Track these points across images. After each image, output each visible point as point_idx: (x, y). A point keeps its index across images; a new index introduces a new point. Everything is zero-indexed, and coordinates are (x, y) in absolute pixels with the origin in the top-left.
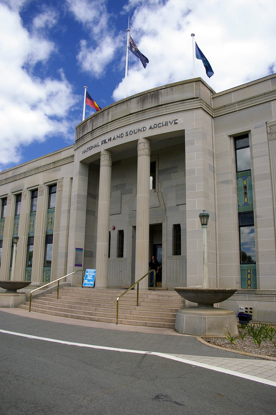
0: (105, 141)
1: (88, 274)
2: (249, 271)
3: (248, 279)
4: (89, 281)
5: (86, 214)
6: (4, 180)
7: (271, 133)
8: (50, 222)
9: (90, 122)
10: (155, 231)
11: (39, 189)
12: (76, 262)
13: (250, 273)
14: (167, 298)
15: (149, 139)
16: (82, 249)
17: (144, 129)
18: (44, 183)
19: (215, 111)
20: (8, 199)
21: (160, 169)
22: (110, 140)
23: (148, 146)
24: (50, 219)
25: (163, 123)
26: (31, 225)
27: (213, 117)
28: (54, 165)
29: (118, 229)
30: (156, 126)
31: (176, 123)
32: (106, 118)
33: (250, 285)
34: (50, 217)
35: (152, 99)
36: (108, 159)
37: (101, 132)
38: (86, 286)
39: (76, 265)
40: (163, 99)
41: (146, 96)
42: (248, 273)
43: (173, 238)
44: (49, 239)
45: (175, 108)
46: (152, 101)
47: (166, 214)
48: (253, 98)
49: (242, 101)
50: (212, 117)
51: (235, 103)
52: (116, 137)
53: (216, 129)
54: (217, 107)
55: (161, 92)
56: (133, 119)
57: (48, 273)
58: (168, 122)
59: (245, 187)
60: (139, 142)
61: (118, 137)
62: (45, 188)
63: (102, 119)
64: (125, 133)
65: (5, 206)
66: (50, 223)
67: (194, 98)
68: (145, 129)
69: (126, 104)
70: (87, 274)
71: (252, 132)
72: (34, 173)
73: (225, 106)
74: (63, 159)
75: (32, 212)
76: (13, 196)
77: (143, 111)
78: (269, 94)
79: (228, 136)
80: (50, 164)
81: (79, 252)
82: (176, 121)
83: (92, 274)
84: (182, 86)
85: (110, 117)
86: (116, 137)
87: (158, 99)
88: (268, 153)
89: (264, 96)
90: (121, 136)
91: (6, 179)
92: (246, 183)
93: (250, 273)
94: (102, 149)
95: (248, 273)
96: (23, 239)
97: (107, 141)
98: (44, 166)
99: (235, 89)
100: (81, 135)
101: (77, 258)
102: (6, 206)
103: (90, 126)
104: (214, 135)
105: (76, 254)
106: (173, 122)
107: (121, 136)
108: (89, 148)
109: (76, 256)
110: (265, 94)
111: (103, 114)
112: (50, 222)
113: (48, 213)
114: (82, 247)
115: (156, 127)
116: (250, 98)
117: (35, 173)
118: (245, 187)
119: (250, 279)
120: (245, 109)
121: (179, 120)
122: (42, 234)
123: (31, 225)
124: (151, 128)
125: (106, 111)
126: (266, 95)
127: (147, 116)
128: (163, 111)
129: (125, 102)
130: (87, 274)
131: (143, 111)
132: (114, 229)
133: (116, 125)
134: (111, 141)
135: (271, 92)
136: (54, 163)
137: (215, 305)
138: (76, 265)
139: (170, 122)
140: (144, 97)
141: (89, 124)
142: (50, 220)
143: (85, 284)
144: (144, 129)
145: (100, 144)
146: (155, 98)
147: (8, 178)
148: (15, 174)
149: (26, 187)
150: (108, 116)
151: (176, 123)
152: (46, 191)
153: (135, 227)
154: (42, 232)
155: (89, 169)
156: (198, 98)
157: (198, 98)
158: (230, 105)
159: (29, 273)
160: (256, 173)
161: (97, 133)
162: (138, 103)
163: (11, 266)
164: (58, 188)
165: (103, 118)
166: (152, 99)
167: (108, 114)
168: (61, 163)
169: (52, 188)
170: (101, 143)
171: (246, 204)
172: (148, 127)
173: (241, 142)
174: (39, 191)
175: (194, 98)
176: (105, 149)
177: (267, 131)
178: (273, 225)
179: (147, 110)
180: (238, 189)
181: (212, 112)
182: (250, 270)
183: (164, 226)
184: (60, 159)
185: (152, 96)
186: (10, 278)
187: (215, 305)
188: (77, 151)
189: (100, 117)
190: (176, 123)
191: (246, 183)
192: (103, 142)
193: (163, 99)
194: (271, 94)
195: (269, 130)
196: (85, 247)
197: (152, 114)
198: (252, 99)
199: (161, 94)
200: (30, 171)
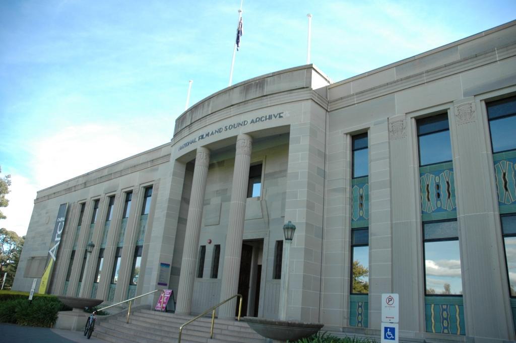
0: (202, 136)
2: (360, 304)
3: (359, 314)
5: (178, 222)
6: (99, 178)
7: (393, 130)
8: (139, 232)
9: (189, 114)
12: (159, 280)
13: (361, 307)
15: (251, 135)
16: (169, 265)
17: (244, 123)
21: (266, 172)
22: (207, 135)
23: (248, 144)
25: (266, 117)
26: (120, 234)
27: (329, 112)
29: (214, 243)
31: (280, 117)
33: (361, 322)
35: (257, 88)
36: (204, 158)
39: (159, 284)
40: (268, 89)
41: (250, 85)
42: (359, 306)
43: (275, 257)
44: (137, 251)
46: (256, 91)
47: (268, 228)
48: (374, 88)
49: (362, 92)
50: (327, 111)
51: (353, 95)
52: (214, 132)
56: (233, 111)
58: (273, 116)
59: (362, 197)
60: (238, 138)
61: (216, 131)
64: (224, 128)
67: (304, 88)
68: (246, 123)
69: (228, 94)
71: (371, 129)
74: (162, 157)
77: (245, 102)
79: (345, 134)
80: (148, 162)
81: (164, 268)
82: (281, 115)
85: (210, 108)
87: (263, 89)
88: (388, 156)
90: (219, 131)
91: (101, 177)
92: (439, 180)
93: (361, 307)
94: (199, 146)
95: (359, 306)
97: (204, 136)
98: (142, 164)
99: (355, 79)
100: (179, 129)
101: (161, 276)
102: (150, 197)
104: (328, 133)
105: (161, 270)
106: (278, 116)
108: (186, 144)
109: (160, 273)
110: (387, 84)
111: (203, 105)
112: (139, 232)
114: (170, 262)
115: (258, 121)
116: (371, 89)
118: (362, 197)
119: (361, 314)
121: (284, 114)
123: (120, 234)
125: (207, 102)
126: (389, 86)
127: (250, 106)
128: (267, 101)
131: (245, 102)
132: (210, 242)
133: (215, 118)
135: (395, 82)
138: (159, 284)
139: (274, 115)
144: (244, 123)
145: (197, 139)
147: (103, 176)
148: (110, 173)
151: (280, 117)
155: (187, 169)
158: (348, 97)
160: (372, 180)
161: (195, 127)
162: (241, 93)
163: (80, 281)
164: (153, 192)
165: (203, 110)
167: (208, 105)
169: (148, 190)
170: (198, 139)
171: (361, 218)
172: (249, 121)
173: (359, 143)
175: (304, 88)
176: (204, 145)
177: (389, 129)
179: (250, 101)
180: (352, 199)
181: (327, 106)
182: (362, 303)
183: (265, 242)
184: (158, 157)
188: (173, 147)
190: (282, 117)
191: (439, 180)
192: (201, 137)
193: (268, 89)
195: (390, 127)
196: (173, 263)
197: (257, 104)
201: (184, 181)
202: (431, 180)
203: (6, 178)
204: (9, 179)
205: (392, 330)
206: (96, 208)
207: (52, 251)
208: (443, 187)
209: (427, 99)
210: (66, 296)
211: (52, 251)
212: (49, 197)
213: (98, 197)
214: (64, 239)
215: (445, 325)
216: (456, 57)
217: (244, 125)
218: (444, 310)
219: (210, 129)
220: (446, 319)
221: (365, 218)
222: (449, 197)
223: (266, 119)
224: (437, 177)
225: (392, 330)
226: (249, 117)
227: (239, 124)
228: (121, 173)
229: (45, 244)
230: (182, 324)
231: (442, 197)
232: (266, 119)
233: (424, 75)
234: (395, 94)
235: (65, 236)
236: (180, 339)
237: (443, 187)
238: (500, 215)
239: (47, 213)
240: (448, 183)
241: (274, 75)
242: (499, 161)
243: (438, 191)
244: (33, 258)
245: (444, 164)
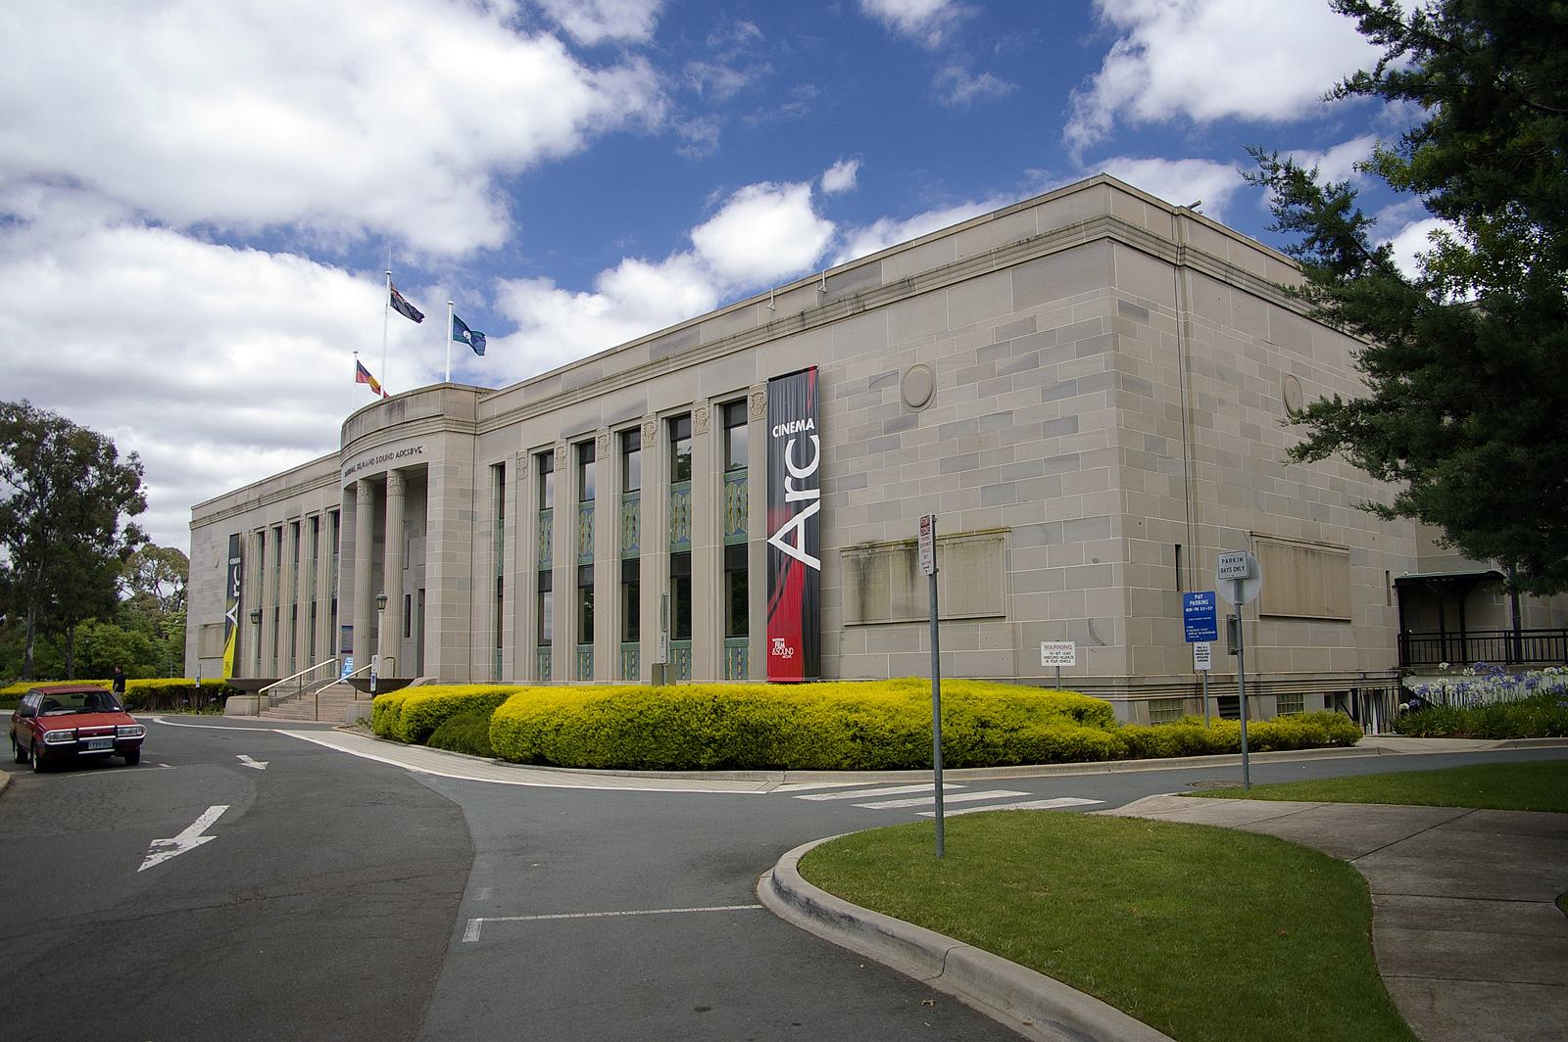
11: (555, 451)
18: (657, 413)
20: (596, 445)
24: (680, 510)
26: (680, 518)
34: (734, 497)
40: (410, 413)
57: (739, 653)
62: (612, 438)
65: (547, 475)
66: (735, 513)
72: (788, 325)
75: (584, 498)
76: (715, 409)
89: (946, 271)
96: (567, 571)
113: (726, 483)
116: (516, 410)
120: (962, 284)
122: (715, 544)
142: (734, 505)
144: (389, 457)
149: (651, 409)
152: (714, 419)
153: (423, 591)
154: (715, 539)
159: (633, 657)
174: (642, 432)
186: (259, 673)
193: (410, 413)
203: (130, 461)
204: (137, 460)
206: (336, 525)
207: (233, 614)
210: (262, 678)
211: (233, 614)
212: (211, 519)
213: (297, 520)
214: (245, 592)
216: (557, 388)
219: (366, 458)
226: (395, 449)
228: (302, 489)
229: (219, 601)
230: (340, 683)
235: (245, 587)
236: (940, 806)
239: (213, 548)
244: (206, 626)
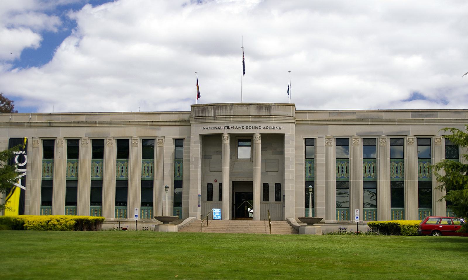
1: (215, 212)
4: (217, 216)
10: (265, 187)
14: (279, 223)
19: (297, 121)
28: (152, 124)
30: (268, 128)
32: (229, 111)
33: (177, 211)
37: (224, 120)
38: (216, 219)
40: (273, 112)
45: (280, 120)
49: (313, 120)
53: (297, 132)
54: (301, 120)
55: (272, 107)
58: (275, 128)
63: (224, 111)
70: (215, 212)
73: (303, 120)
78: (328, 121)
82: (280, 128)
83: (218, 212)
84: (284, 106)
86: (238, 127)
103: (212, 112)
107: (242, 128)
116: (318, 120)
117: (124, 125)
118: (310, 167)
121: (282, 127)
124: (264, 128)
129: (246, 105)
130: (215, 212)
134: (233, 128)
136: (152, 122)
137: (314, 224)
140: (260, 107)
141: (211, 109)
143: (215, 218)
144: (259, 128)
146: (267, 110)
150: (231, 110)
156: (293, 116)
157: (293, 116)
165: (226, 111)
166: (265, 109)
167: (231, 109)
168: (160, 124)
171: (179, 176)
178: (170, 115)
180: (306, 168)
185: (266, 108)
187: (314, 224)
189: (223, 109)
190: (280, 129)
193: (273, 112)
194: (329, 121)
198: (319, 121)
199: (272, 109)
200: (118, 123)
201: (202, 149)
202: (340, 165)
205: (358, 217)
208: (124, 168)
209: (343, 131)
215: (343, 218)
217: (259, 129)
218: (342, 213)
220: (343, 216)
221: (314, 177)
222: (346, 172)
223: (272, 128)
224: (73, 164)
225: (358, 217)
226: (262, 125)
227: (256, 127)
231: (99, 172)
232: (272, 128)
233: (98, 123)
234: (329, 126)
237: (124, 168)
238: (363, 181)
240: (152, 167)
241: (275, 105)
242: (93, 162)
243: (397, 170)
245: (428, 159)
